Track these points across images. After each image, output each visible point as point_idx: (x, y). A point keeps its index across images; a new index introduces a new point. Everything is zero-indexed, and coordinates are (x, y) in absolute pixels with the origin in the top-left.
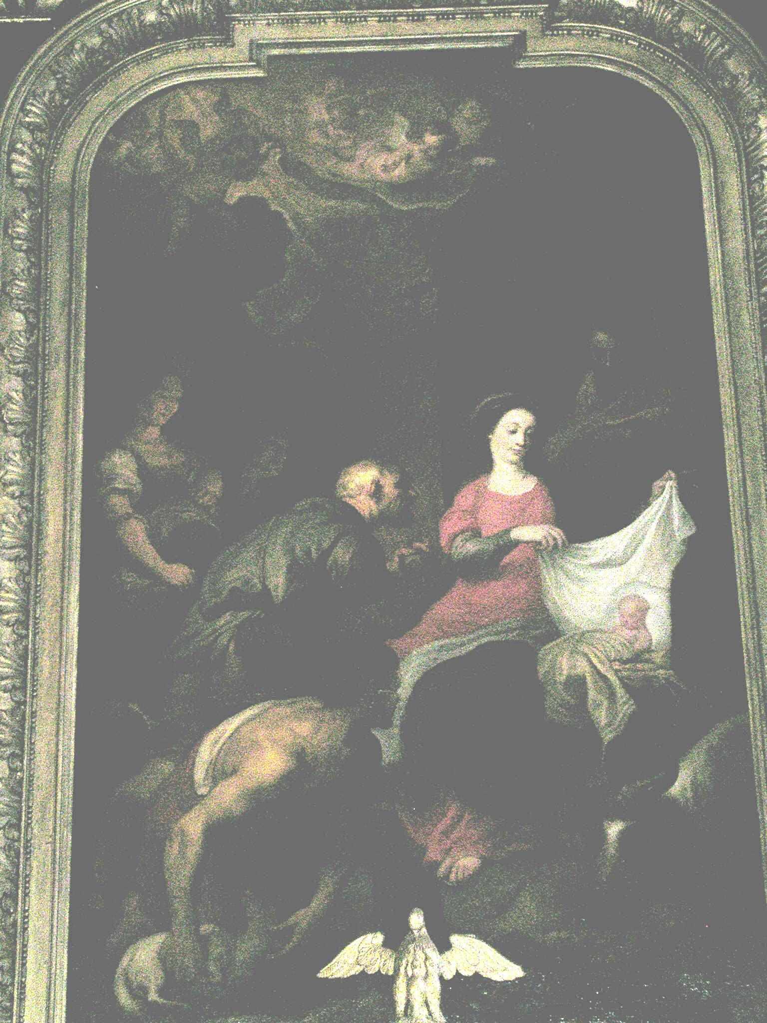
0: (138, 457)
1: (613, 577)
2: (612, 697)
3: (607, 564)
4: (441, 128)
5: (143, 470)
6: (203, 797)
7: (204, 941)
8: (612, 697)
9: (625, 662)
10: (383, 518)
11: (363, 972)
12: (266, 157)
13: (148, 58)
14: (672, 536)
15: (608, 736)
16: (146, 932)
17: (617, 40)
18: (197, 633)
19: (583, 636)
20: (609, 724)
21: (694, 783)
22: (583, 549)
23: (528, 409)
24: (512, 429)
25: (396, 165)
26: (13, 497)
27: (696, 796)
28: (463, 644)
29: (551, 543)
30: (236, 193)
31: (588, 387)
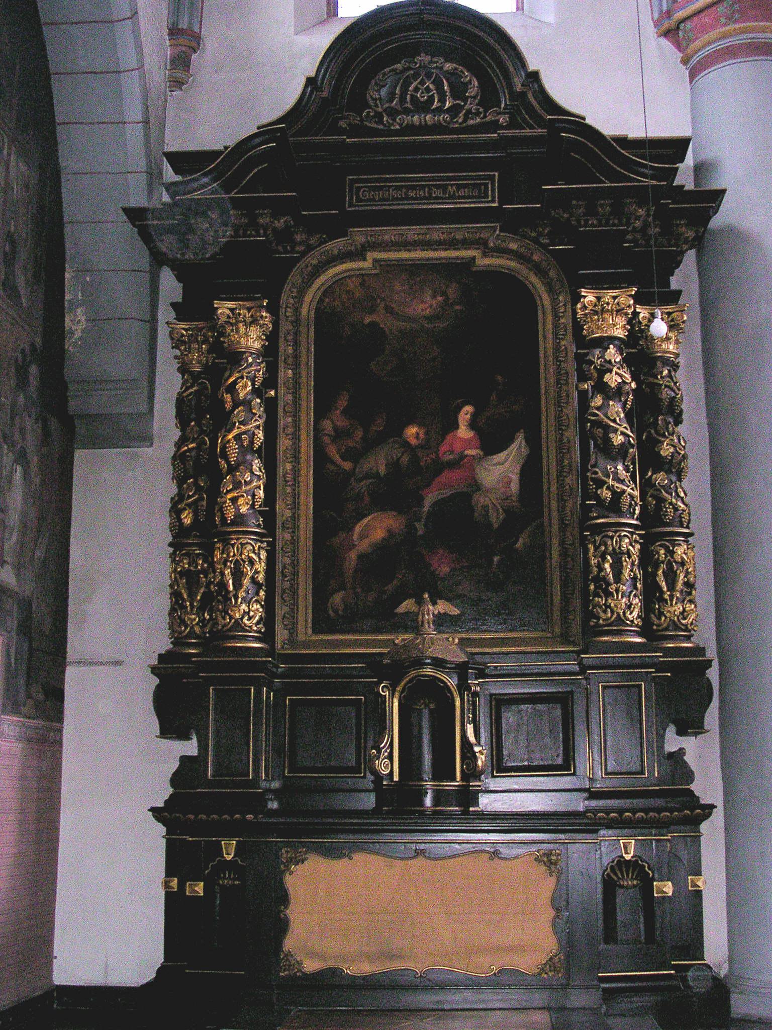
1: (499, 470)
3: (499, 464)
4: (444, 294)
5: (336, 429)
10: (421, 446)
13: (335, 266)
15: (496, 526)
23: (472, 405)
26: (289, 439)
30: (367, 320)
31: (494, 396)
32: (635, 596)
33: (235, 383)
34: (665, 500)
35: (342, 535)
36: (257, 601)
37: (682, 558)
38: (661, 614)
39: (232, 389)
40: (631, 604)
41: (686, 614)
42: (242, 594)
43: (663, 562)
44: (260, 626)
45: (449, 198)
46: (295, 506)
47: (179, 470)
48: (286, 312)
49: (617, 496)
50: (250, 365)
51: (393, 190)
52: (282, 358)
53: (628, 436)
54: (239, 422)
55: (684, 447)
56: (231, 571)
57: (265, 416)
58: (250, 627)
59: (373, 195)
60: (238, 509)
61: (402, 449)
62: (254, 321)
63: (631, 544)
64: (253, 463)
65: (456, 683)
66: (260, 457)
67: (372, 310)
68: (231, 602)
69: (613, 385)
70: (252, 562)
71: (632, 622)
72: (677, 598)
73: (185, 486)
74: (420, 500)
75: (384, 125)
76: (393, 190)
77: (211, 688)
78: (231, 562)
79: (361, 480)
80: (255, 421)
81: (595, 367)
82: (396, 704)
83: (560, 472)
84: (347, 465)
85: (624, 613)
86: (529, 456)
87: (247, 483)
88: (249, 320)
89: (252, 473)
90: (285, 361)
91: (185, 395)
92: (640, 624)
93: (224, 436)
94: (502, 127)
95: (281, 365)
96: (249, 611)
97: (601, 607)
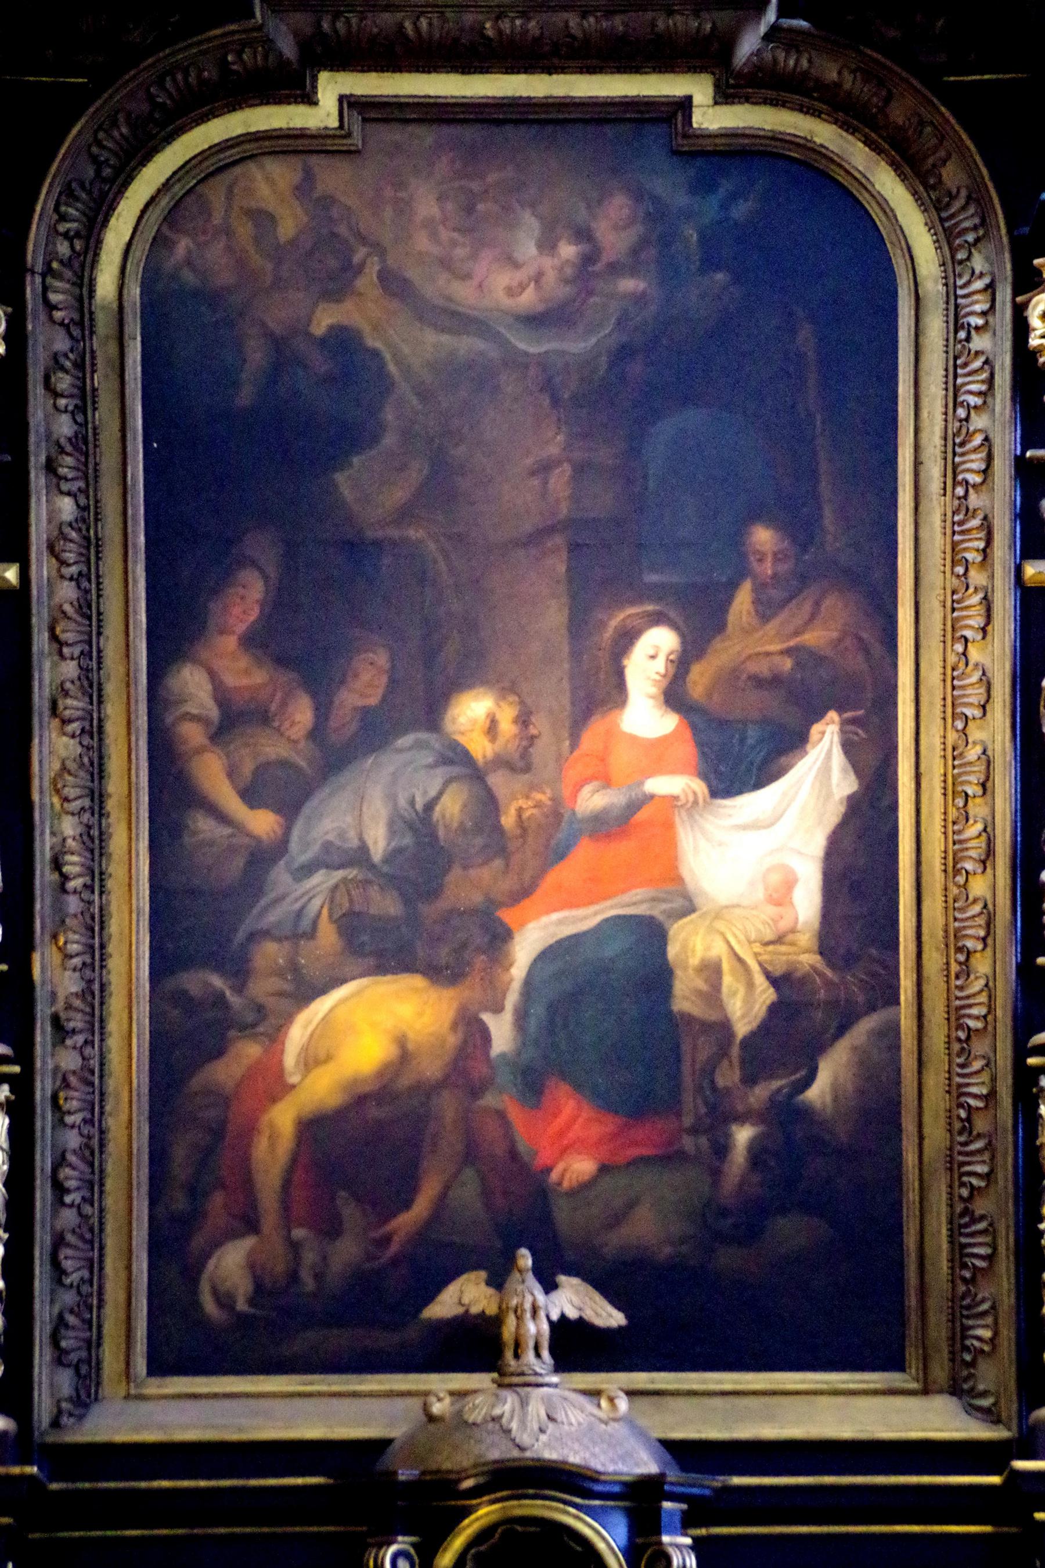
0: (212, 675)
2: (750, 985)
4: (583, 234)
6: (293, 1087)
7: (295, 1247)
8: (750, 985)
10: (501, 762)
11: (467, 1311)
12: (360, 269)
14: (829, 795)
16: (232, 1235)
17: (973, 1364)
19: (718, 915)
20: (743, 1016)
21: (835, 1087)
22: (725, 807)
24: (652, 652)
25: (522, 287)
27: (835, 1099)
28: (585, 918)
29: (691, 798)
35: (249, 1051)
52: (37, 459)
79: (308, 870)
86: (854, 806)
90: (50, 467)
95: (37, 480)
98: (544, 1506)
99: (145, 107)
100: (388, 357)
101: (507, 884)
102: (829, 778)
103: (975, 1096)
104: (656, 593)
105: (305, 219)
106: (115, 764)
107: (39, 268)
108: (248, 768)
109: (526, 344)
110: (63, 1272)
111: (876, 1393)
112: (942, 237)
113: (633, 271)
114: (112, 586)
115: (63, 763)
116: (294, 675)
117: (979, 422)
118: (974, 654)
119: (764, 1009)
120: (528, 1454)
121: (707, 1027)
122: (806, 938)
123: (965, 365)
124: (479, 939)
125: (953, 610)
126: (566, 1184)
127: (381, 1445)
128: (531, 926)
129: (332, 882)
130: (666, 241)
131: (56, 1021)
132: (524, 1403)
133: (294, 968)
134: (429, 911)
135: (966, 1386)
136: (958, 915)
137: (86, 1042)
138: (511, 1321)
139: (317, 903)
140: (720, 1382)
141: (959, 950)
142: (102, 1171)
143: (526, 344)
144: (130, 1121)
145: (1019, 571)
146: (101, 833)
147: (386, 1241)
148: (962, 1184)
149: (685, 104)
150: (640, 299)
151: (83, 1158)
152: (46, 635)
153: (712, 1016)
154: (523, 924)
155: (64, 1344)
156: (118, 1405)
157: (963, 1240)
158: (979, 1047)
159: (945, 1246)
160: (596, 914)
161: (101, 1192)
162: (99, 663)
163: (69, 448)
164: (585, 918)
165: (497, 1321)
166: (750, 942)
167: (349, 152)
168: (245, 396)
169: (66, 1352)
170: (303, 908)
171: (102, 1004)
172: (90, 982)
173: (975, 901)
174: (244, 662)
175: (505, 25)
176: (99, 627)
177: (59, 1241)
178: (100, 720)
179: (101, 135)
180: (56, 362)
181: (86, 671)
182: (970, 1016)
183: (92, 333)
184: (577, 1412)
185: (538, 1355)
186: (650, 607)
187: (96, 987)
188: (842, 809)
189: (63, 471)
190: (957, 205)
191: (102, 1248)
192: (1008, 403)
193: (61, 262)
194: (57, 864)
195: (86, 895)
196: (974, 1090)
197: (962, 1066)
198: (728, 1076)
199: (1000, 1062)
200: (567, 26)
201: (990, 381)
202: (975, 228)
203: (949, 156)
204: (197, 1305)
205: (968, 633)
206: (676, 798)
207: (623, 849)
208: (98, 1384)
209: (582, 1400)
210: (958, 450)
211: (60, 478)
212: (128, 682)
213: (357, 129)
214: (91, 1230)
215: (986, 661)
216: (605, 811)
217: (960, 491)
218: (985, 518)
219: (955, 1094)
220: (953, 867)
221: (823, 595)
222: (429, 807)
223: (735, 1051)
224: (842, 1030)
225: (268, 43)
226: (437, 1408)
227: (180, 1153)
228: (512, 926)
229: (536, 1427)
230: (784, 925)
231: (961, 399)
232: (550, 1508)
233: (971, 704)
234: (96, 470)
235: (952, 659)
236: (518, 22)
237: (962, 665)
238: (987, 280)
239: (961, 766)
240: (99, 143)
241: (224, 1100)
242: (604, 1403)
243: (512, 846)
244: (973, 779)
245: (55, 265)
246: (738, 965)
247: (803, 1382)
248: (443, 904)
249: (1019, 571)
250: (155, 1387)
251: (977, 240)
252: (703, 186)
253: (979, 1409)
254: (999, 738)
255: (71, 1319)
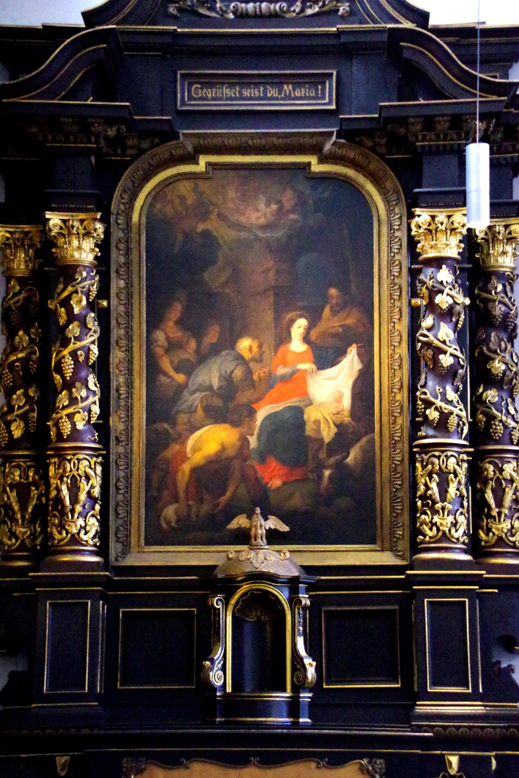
0: (166, 334)
2: (329, 427)
3: (332, 378)
4: (279, 202)
5: (168, 338)
7: (189, 506)
8: (329, 427)
9: (335, 414)
10: (253, 359)
11: (240, 527)
12: (211, 212)
14: (353, 368)
16: (171, 503)
17: (396, 542)
18: (187, 400)
19: (320, 405)
20: (327, 437)
21: (355, 458)
24: (299, 326)
25: (260, 218)
27: (355, 461)
28: (279, 407)
29: (311, 370)
30: (201, 227)
32: (462, 513)
33: (69, 298)
34: (494, 418)
35: (176, 447)
36: (93, 516)
37: (511, 475)
38: (489, 530)
39: (66, 303)
40: (457, 522)
41: (514, 531)
42: (78, 508)
43: (492, 479)
44: (96, 540)
45: (282, 99)
46: (129, 418)
47: (9, 380)
48: (117, 219)
49: (445, 417)
50: (84, 280)
51: (226, 88)
52: (113, 268)
53: (458, 357)
54: (74, 337)
55: (516, 364)
56: (68, 486)
57: (99, 330)
58: (87, 541)
59: (205, 94)
60: (74, 425)
61: (235, 362)
62: (87, 234)
63: (458, 464)
64: (89, 379)
65: (287, 597)
66: (94, 371)
67: (204, 217)
68: (68, 517)
69: (444, 306)
70: (88, 478)
71: (458, 539)
72: (506, 515)
73: (15, 397)
74: (252, 413)
75: (217, 13)
76: (226, 88)
77: (48, 602)
78: (67, 477)
79: (193, 393)
80: (91, 336)
81: (427, 288)
82: (229, 619)
83: (392, 389)
84: (180, 378)
85: (450, 531)
86: (361, 371)
87: (83, 400)
88: (82, 232)
89: (88, 388)
90: (117, 272)
91: (12, 302)
92: (467, 541)
93: (59, 352)
94: (343, 19)
95: (113, 275)
96: (86, 526)
97: (427, 525)
98: (273, 589)
99: (148, 166)
100: (220, 239)
101: (256, 396)
102: (353, 365)
103: (397, 461)
104: (303, 308)
105: (195, 197)
106: (136, 361)
107: (115, 211)
108: (176, 361)
109: (261, 234)
110: (119, 514)
111: (367, 551)
112: (386, 203)
113: (293, 212)
114: (136, 306)
115: (120, 359)
116: (191, 333)
117: (397, 257)
118: (397, 327)
119: (334, 434)
120: (258, 570)
121: (316, 440)
122: (346, 413)
123: (393, 240)
124: (245, 413)
125: (391, 313)
126: (272, 488)
127: (214, 567)
128: (262, 409)
129: (201, 396)
130: (305, 203)
131: (117, 438)
132: (257, 554)
133: (189, 422)
134: (231, 405)
135: (394, 549)
136: (392, 405)
137: (126, 444)
138: (254, 529)
139: (197, 402)
140: (320, 548)
141: (393, 416)
142: (131, 483)
143: (261, 234)
144: (140, 469)
145: (410, 302)
146: (131, 381)
147: (217, 505)
148: (394, 487)
149: (309, 164)
150: (295, 221)
151: (125, 479)
152: (115, 321)
153: (318, 437)
154: (260, 408)
155: (119, 536)
156: (135, 554)
157: (394, 504)
158: (399, 445)
159: (389, 506)
160: (282, 405)
161: (131, 490)
162: (131, 330)
163: (123, 266)
164: (279, 407)
165: (250, 529)
166: (329, 414)
167: (208, 179)
168: (177, 249)
169: (119, 538)
170: (192, 404)
171: (131, 433)
172: (128, 426)
173: (397, 401)
174: (175, 329)
175: (255, 141)
176: (132, 319)
177: (117, 505)
178: (131, 347)
179: (134, 174)
180: (120, 241)
181: (127, 332)
182: (396, 436)
183: (131, 232)
184: (273, 557)
185: (262, 540)
186: (299, 313)
187: (130, 428)
188: (357, 373)
189: (121, 272)
190: (390, 193)
191: (131, 507)
192: (406, 251)
193: (122, 211)
194: (117, 390)
195: (126, 400)
196: (397, 459)
197: (394, 451)
198: (322, 455)
199: (405, 450)
200: (273, 141)
201: (401, 245)
202: (396, 200)
203: (388, 179)
204: (160, 525)
205: (395, 320)
206: (307, 370)
207: (289, 387)
208: (130, 548)
209: (275, 553)
210: (392, 265)
211: (120, 274)
212: (140, 335)
213: (211, 172)
214: (128, 501)
215: (400, 329)
216: (285, 374)
217: (392, 278)
218: (400, 286)
219: (391, 460)
220: (391, 390)
221: (352, 309)
222: (232, 373)
223: (325, 447)
224: (358, 440)
225: (184, 147)
226: (231, 556)
227: (155, 478)
228: (256, 409)
229: (260, 562)
230: (339, 409)
231: (392, 250)
232: (266, 586)
233: (396, 342)
234: (131, 272)
235: (390, 328)
236: (259, 141)
237: (393, 329)
238: (399, 215)
239: (393, 360)
240: (133, 176)
241: (167, 462)
242: (282, 554)
243: (256, 385)
244: (397, 364)
245: (120, 212)
246: (326, 421)
247: (345, 548)
248: (235, 403)
249: (410, 302)
250: (147, 549)
251: (396, 204)
252: (314, 188)
253: (399, 555)
254: (404, 352)
255: (121, 528)
